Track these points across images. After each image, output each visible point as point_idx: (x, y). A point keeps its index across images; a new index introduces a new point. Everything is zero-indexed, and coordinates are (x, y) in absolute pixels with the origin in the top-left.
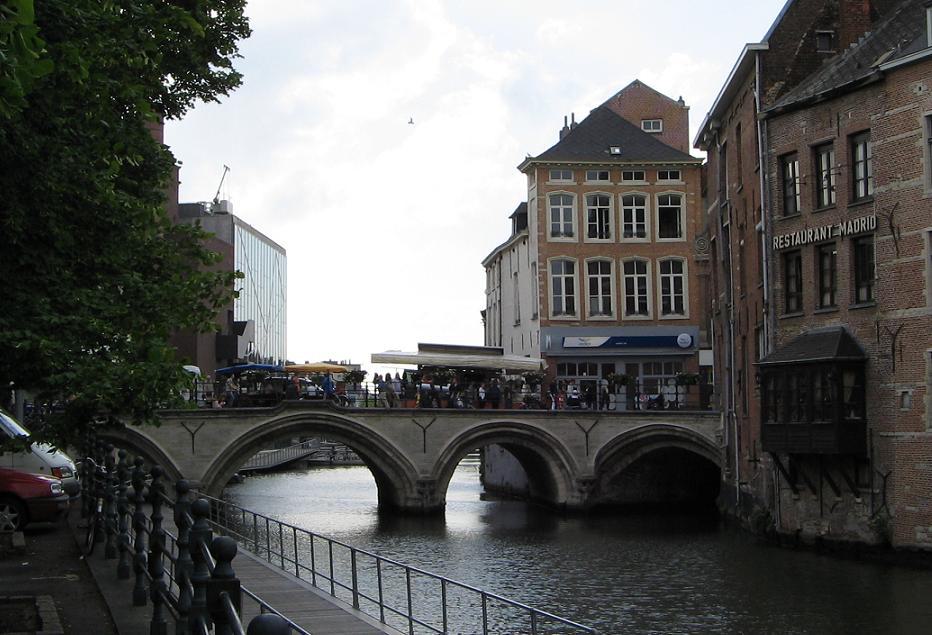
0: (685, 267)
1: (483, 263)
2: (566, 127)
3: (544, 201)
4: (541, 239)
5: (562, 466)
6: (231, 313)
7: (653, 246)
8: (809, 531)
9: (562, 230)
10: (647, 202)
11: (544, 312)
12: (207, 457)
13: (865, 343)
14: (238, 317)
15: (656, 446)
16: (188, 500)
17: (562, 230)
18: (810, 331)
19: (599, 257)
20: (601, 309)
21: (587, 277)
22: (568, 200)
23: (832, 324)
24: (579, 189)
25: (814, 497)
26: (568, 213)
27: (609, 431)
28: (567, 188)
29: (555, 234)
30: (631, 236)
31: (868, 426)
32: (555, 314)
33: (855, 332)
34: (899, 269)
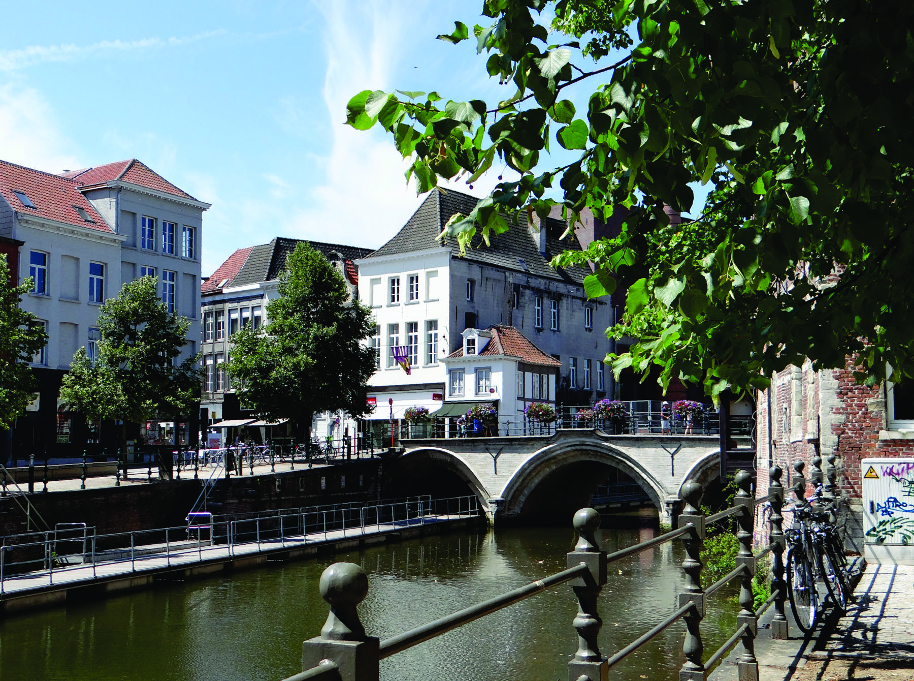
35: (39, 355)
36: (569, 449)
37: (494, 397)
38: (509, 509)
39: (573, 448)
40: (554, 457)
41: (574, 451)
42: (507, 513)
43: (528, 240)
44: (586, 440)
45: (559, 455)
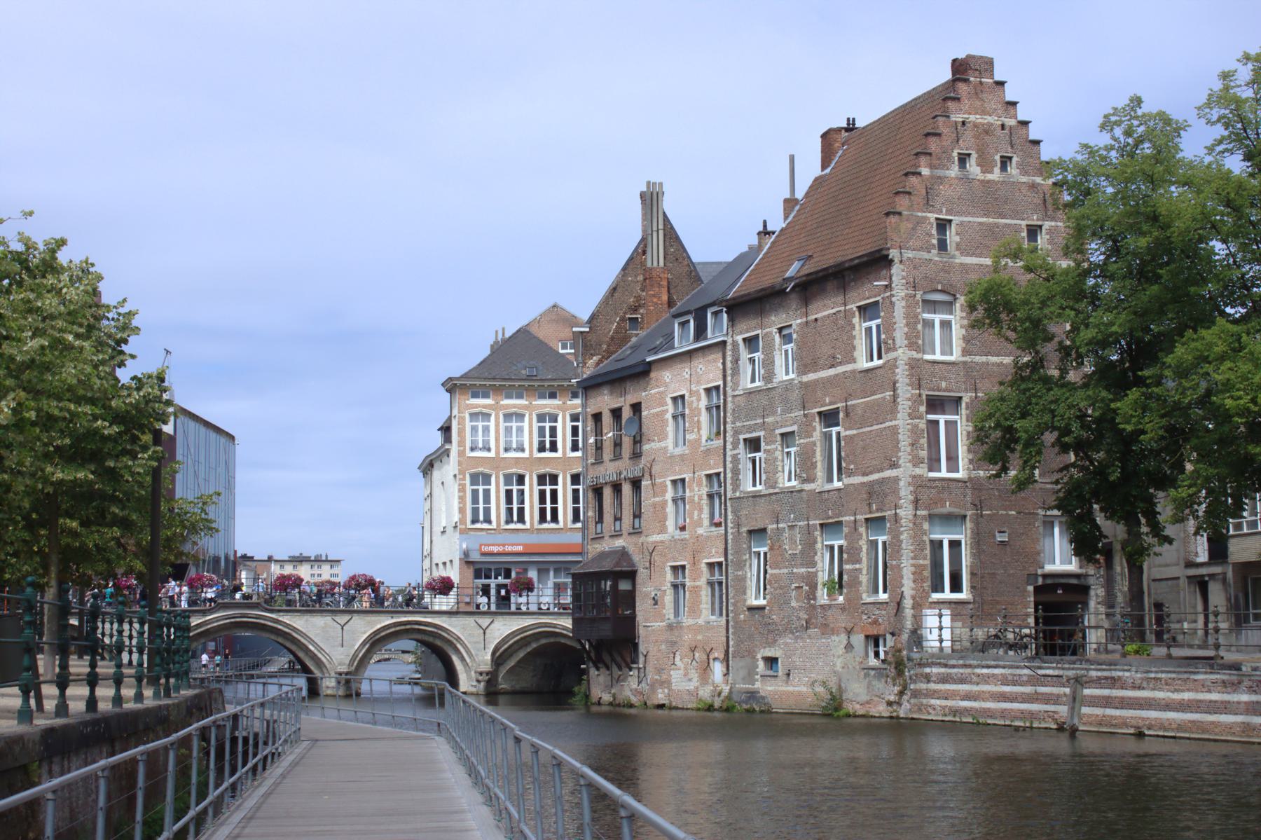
2: (496, 342)
3: (463, 418)
4: (461, 454)
5: (463, 659)
7: (565, 459)
10: (560, 419)
11: (462, 520)
13: (636, 558)
15: (543, 641)
20: (481, 518)
21: (503, 489)
22: (486, 416)
23: (619, 543)
24: (496, 407)
26: (486, 429)
27: (503, 628)
28: (485, 406)
32: (474, 522)
33: (631, 550)
34: (654, 505)
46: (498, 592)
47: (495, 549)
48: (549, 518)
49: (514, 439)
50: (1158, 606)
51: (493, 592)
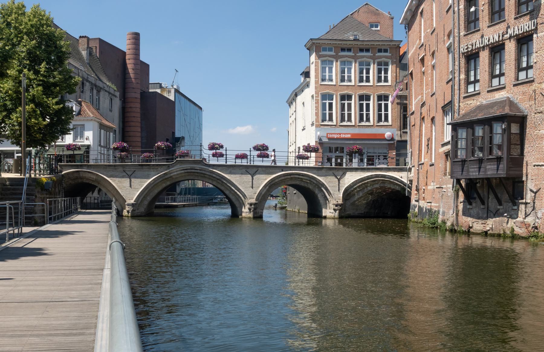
0: (390, 99)
1: (287, 102)
4: (316, 82)
6: (174, 133)
8: (478, 228)
9: (327, 78)
11: (317, 120)
12: (136, 188)
14: (177, 135)
16: (88, 201)
17: (327, 78)
18: (484, 102)
19: (345, 92)
25: (482, 207)
29: (323, 80)
30: (363, 82)
31: (525, 160)
32: (323, 121)
35: (461, 50)
36: (183, 171)
37: (87, 143)
38: (138, 209)
39: (186, 171)
40: (171, 177)
41: (185, 173)
42: (137, 211)
43: (79, 53)
44: (195, 166)
45: (175, 175)
46: (336, 160)
47: (336, 136)
48: (346, 119)
49: (327, 74)
50: (237, 157)
51: (333, 160)
